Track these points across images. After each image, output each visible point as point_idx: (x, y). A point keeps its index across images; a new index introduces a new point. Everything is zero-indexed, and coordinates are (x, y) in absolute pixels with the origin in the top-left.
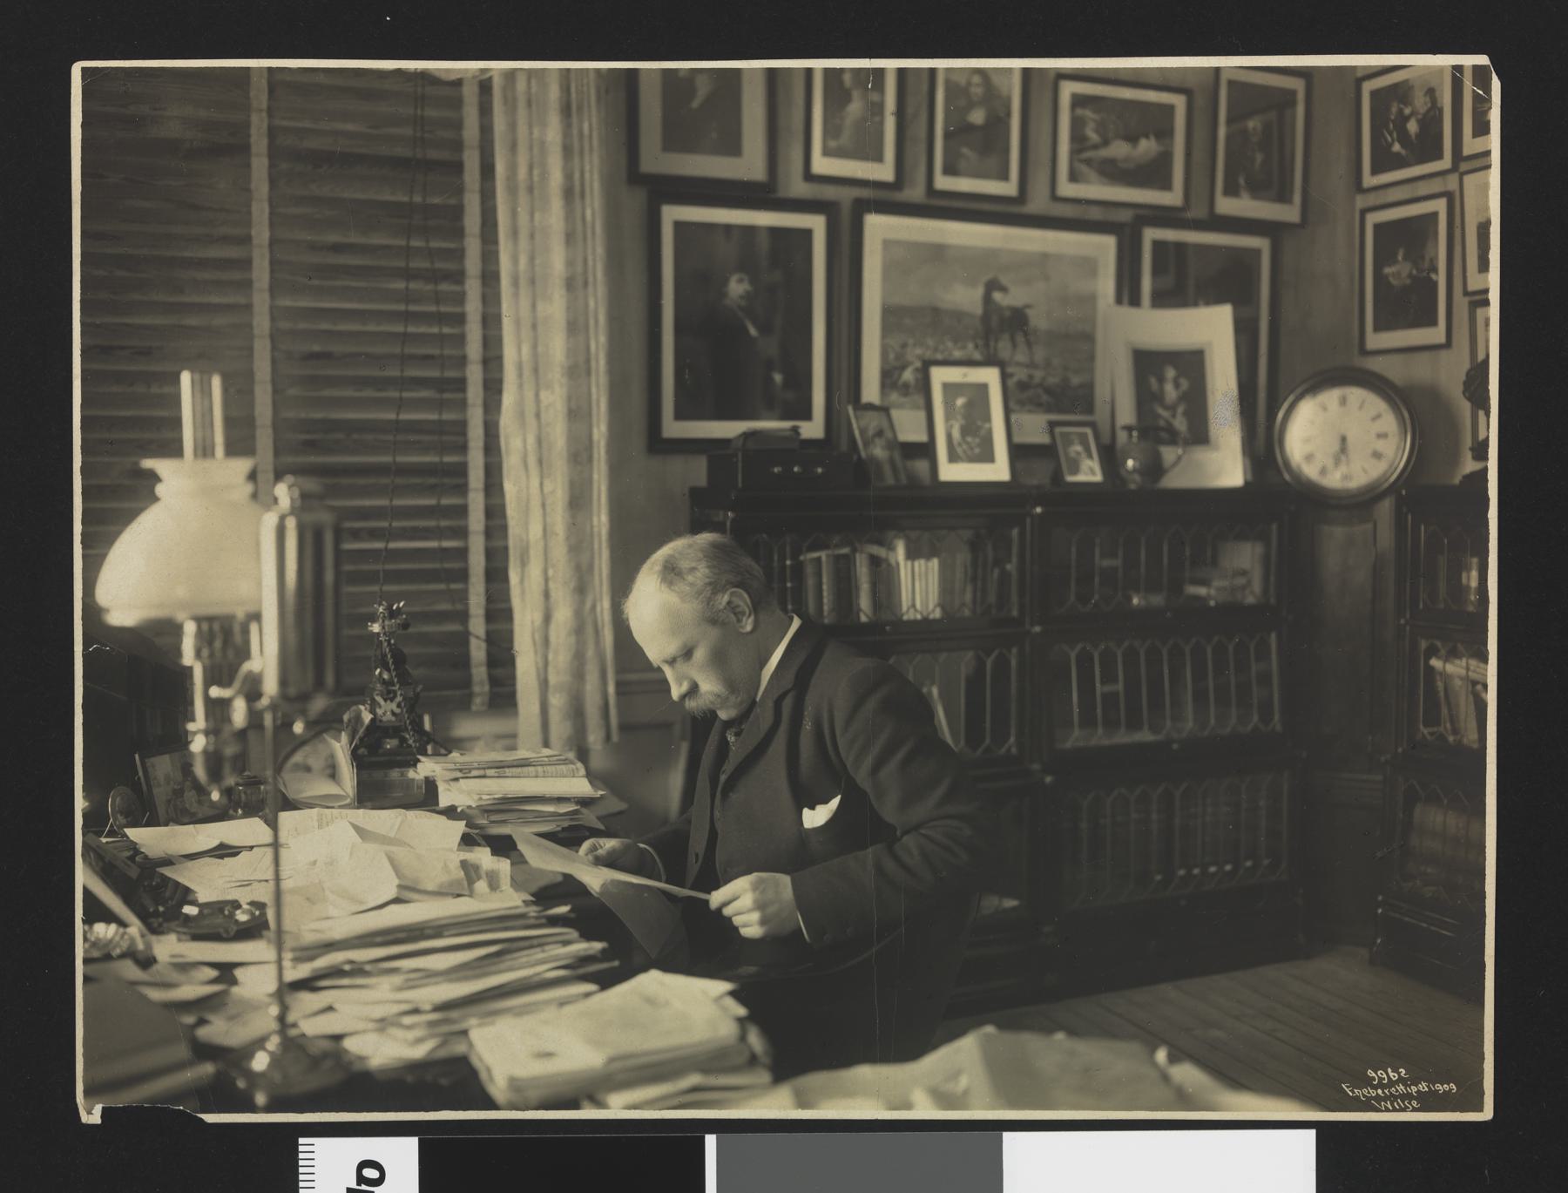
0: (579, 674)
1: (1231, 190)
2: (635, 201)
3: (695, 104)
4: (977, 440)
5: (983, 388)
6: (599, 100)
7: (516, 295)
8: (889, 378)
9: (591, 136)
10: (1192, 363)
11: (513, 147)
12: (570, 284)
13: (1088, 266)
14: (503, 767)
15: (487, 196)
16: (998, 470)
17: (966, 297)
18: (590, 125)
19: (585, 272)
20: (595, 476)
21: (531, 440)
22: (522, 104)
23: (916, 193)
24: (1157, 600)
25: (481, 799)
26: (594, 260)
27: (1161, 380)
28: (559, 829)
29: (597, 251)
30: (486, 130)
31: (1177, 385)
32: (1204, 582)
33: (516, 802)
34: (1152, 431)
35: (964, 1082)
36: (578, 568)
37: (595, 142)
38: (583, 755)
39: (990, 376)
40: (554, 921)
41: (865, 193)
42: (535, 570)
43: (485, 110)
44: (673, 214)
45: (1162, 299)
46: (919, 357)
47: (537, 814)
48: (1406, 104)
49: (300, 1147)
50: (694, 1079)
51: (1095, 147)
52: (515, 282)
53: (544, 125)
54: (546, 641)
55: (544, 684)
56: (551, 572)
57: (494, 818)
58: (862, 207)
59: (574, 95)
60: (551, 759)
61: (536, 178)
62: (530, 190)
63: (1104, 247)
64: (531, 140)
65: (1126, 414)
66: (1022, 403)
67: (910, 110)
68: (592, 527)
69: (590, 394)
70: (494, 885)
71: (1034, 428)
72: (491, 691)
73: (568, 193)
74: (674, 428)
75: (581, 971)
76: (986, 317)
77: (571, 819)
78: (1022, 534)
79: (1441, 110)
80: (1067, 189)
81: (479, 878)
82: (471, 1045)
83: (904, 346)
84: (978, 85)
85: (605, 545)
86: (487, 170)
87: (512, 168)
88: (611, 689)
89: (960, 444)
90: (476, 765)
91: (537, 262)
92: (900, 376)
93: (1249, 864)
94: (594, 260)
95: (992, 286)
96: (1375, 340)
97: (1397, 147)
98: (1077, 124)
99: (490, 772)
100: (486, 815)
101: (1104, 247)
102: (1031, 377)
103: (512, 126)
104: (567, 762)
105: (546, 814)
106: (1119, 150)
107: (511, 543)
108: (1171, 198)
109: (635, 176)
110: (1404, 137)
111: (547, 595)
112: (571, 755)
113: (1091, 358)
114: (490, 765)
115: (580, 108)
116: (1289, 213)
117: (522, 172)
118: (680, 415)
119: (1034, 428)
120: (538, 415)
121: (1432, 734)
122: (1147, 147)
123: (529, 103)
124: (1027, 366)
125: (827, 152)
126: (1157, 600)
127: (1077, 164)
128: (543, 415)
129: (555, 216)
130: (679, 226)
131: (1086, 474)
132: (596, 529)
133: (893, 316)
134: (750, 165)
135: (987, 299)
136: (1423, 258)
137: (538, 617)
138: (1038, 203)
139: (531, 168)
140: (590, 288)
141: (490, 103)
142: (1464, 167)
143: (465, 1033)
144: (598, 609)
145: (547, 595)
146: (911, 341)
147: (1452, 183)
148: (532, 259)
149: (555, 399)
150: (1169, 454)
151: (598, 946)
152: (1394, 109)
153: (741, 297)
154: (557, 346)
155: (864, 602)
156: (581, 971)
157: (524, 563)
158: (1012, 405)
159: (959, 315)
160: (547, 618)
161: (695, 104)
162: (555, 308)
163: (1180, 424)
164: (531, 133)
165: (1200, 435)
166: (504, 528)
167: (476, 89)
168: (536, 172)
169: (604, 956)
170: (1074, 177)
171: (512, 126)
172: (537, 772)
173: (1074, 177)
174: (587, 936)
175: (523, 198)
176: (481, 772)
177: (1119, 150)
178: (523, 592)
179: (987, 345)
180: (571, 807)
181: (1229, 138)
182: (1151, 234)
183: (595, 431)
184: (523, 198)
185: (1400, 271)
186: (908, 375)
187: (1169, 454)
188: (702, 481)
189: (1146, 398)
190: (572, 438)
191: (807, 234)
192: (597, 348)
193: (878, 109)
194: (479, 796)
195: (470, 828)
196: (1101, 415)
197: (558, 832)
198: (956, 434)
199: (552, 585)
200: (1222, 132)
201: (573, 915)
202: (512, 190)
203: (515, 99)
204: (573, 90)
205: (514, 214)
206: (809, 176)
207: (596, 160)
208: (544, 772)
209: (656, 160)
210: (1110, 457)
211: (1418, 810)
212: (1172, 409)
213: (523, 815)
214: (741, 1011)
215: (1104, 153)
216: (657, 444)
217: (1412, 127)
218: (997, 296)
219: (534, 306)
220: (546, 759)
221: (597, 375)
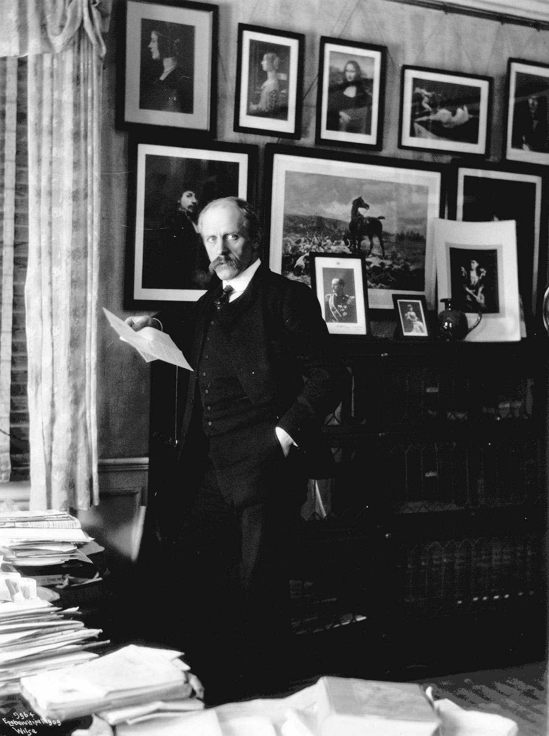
0: (73, 459)
1: (517, 144)
2: (118, 142)
3: (162, 78)
4: (345, 307)
5: (350, 273)
6: (99, 74)
7: (39, 202)
9: (92, 99)
11: (40, 103)
12: (75, 196)
13: (423, 190)
14: (27, 522)
15: (21, 134)
16: (359, 327)
17: (341, 212)
18: (93, 91)
19: (86, 189)
20: (88, 325)
21: (46, 300)
22: (46, 75)
25: (12, 541)
26: (92, 181)
27: (469, 269)
28: (63, 562)
29: (95, 172)
30: (22, 91)
31: (479, 273)
33: (35, 544)
35: (316, 708)
36: (75, 387)
37: (95, 102)
38: (74, 512)
39: (355, 265)
40: (67, 617)
42: (45, 388)
43: (21, 76)
44: (145, 150)
45: (471, 215)
46: (308, 249)
47: (47, 552)
50: (159, 705)
51: (428, 114)
52: (39, 194)
53: (61, 90)
54: (51, 436)
55: (49, 465)
56: (56, 390)
57: (20, 554)
59: (82, 71)
60: (58, 516)
61: (55, 125)
62: (51, 133)
63: (433, 179)
64: (52, 99)
65: (445, 292)
66: (376, 282)
67: (306, 86)
68: (85, 360)
69: (86, 271)
70: (26, 595)
71: (383, 298)
72: (12, 470)
73: (76, 135)
74: (141, 293)
75: (87, 646)
76: (353, 225)
77: (71, 556)
80: (408, 141)
81: (17, 591)
82: (22, 688)
83: (299, 242)
84: (352, 71)
85: (93, 371)
86: (22, 117)
87: (39, 117)
88: (95, 469)
89: (334, 310)
90: (9, 520)
91: (54, 180)
92: (295, 263)
94: (92, 181)
95: (359, 203)
98: (417, 98)
99: (18, 524)
100: (15, 552)
101: (433, 179)
102: (382, 264)
103: (40, 90)
104: (69, 518)
105: (53, 552)
106: (443, 114)
107: (30, 369)
108: (478, 148)
111: (53, 405)
112: (67, 514)
113: (424, 253)
114: (18, 520)
115: (86, 80)
117: (46, 121)
118: (146, 285)
119: (383, 298)
120: (51, 283)
122: (462, 114)
123: (52, 75)
124: (381, 257)
125: (250, 113)
127: (416, 126)
128: (54, 283)
129: (66, 151)
130: (150, 158)
131: (417, 331)
132: (87, 361)
133: (293, 225)
134: (199, 119)
135: (355, 211)
137: (47, 420)
138: (390, 149)
139: (52, 118)
140: (89, 199)
141: (25, 72)
143: (18, 680)
144: (88, 415)
145: (53, 405)
148: (50, 179)
149: (63, 272)
150: (472, 318)
151: (95, 632)
153: (190, 207)
154: (65, 239)
156: (87, 646)
157: (37, 383)
158: (369, 283)
159: (335, 223)
160: (53, 421)
161: (162, 78)
162: (65, 211)
163: (480, 298)
164: (53, 95)
165: (492, 306)
166: (24, 359)
167: (16, 63)
168: (55, 121)
169: (101, 637)
170: (413, 134)
171: (40, 90)
172: (49, 525)
173: (413, 134)
174: (88, 626)
175: (46, 139)
176: (12, 525)
177: (443, 114)
178: (36, 402)
179: (353, 243)
180: (72, 548)
181: (516, 106)
183: (89, 295)
184: (46, 139)
186: (300, 262)
187: (472, 318)
189: (458, 280)
190: (74, 299)
191: (236, 166)
192: (92, 239)
193: (284, 85)
194: (11, 540)
195: (5, 561)
196: (428, 292)
197: (63, 564)
198: (332, 304)
199: (56, 398)
200: (512, 101)
201: (80, 613)
202: (39, 132)
203: (42, 72)
204: (82, 67)
205: (39, 147)
206: (238, 128)
207: (96, 115)
208: (54, 525)
209: (135, 114)
210: (433, 320)
212: (475, 288)
213: (38, 552)
214: (187, 667)
215: (432, 117)
218: (361, 210)
219: (50, 210)
220: (56, 517)
221: (92, 257)
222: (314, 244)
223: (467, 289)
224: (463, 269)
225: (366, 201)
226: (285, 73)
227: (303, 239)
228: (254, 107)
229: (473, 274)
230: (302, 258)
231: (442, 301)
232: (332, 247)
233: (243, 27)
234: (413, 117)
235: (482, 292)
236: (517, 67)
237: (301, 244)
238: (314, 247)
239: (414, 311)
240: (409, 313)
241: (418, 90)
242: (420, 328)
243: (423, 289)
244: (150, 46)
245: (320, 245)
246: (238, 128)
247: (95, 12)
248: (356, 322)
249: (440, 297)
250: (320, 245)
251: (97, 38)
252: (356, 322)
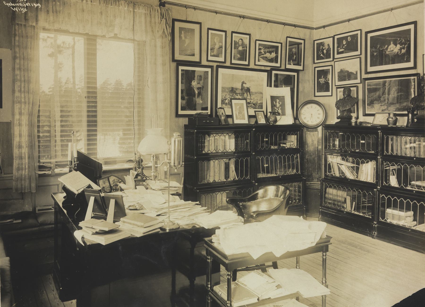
31: (279, 103)
51: (263, 54)
71: (252, 112)
74: (181, 112)
83: (226, 95)
95: (243, 83)
98: (260, 49)
108: (278, 65)
122: (273, 55)
135: (242, 85)
136: (327, 78)
146: (227, 94)
147: (332, 63)
150: (278, 117)
173: (259, 61)
182: (274, 72)
186: (227, 101)
187: (278, 117)
196: (264, 109)
215: (265, 55)
223: (276, 108)
224: (274, 102)
226: (297, 120)
227: (227, 94)
228: (212, 54)
229: (277, 104)
231: (269, 112)
232: (236, 96)
233: (209, 29)
234: (259, 55)
235: (280, 109)
236: (289, 39)
237: (227, 96)
238: (231, 97)
239: (261, 116)
241: (260, 47)
242: (263, 121)
243: (262, 109)
245: (232, 96)
247: (167, 26)
248: (181, 110)
249: (268, 111)
250: (232, 96)
251: (168, 34)
252: (181, 110)
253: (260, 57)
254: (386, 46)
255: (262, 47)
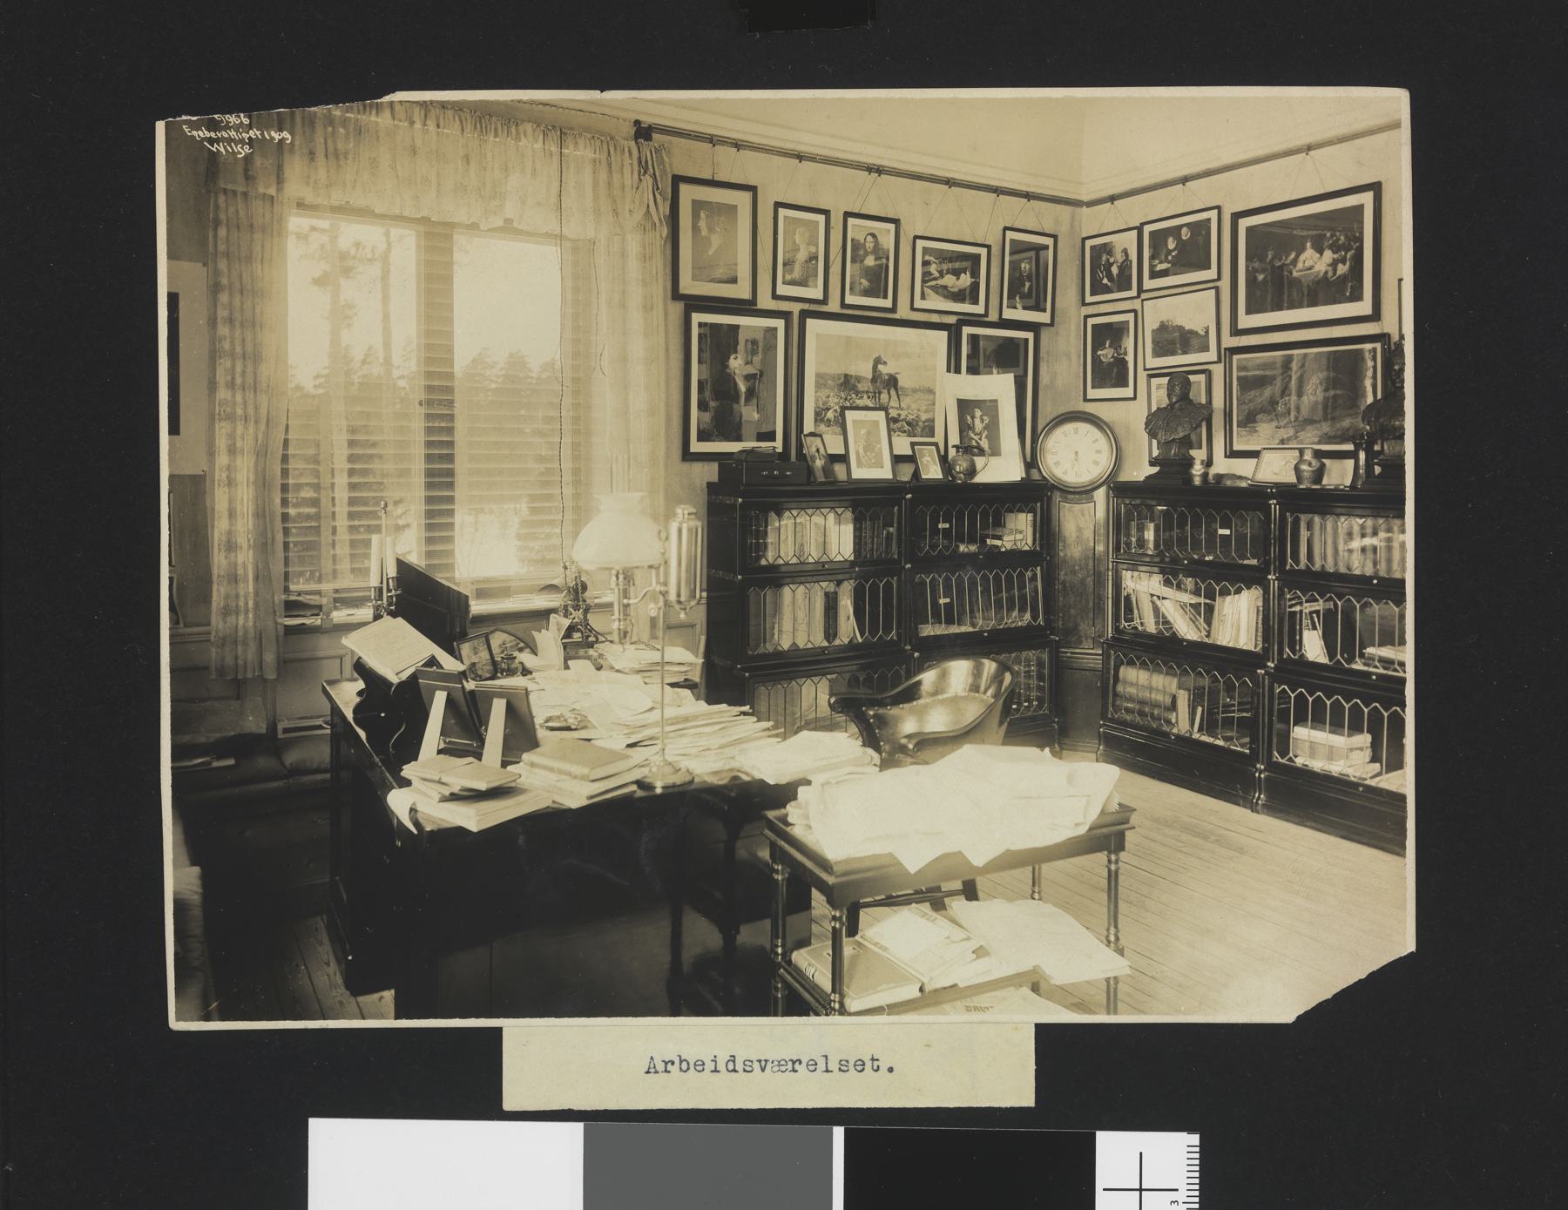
2: (677, 308)
8: (819, 416)
10: (991, 407)
23: (833, 306)
24: (973, 548)
31: (982, 421)
32: (999, 538)
34: (966, 449)
41: (806, 306)
45: (973, 370)
48: (1111, 256)
49: (1198, 1144)
51: (935, 279)
58: (805, 315)
65: (954, 439)
71: (903, 446)
74: (696, 447)
78: (900, 511)
79: (1131, 261)
83: (828, 397)
93: (1026, 704)
95: (878, 361)
96: (1092, 394)
97: (1105, 281)
98: (925, 263)
106: (949, 280)
108: (979, 309)
109: (676, 295)
110: (1110, 276)
116: (1043, 317)
121: (1129, 626)
122: (965, 280)
126: (973, 548)
136: (1120, 347)
142: (1144, 296)
146: (832, 394)
147: (1136, 304)
150: (979, 462)
152: (1104, 258)
155: (1330, 559)
173: (923, 297)
177: (949, 280)
185: (1107, 354)
186: (830, 415)
187: (979, 462)
188: (715, 478)
189: (964, 428)
196: (939, 437)
198: (861, 451)
211: (1122, 669)
215: (941, 282)
216: (687, 456)
217: (1115, 270)
218: (881, 367)
222: (841, 398)
223: (972, 435)
224: (969, 417)
225: (884, 359)
227: (832, 394)
228: (788, 277)
229: (977, 421)
230: (831, 411)
231: (953, 446)
232: (856, 401)
233: (778, 205)
234: (924, 282)
235: (986, 437)
236: (1010, 235)
238: (841, 401)
239: (929, 456)
240: (926, 458)
241: (927, 258)
244: (699, 224)
246: (775, 296)
248: (1038, 1026)
251: (660, 219)
253: (927, 287)
254: (1293, 256)
255: (932, 258)
